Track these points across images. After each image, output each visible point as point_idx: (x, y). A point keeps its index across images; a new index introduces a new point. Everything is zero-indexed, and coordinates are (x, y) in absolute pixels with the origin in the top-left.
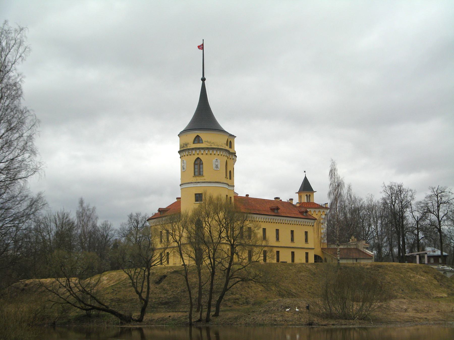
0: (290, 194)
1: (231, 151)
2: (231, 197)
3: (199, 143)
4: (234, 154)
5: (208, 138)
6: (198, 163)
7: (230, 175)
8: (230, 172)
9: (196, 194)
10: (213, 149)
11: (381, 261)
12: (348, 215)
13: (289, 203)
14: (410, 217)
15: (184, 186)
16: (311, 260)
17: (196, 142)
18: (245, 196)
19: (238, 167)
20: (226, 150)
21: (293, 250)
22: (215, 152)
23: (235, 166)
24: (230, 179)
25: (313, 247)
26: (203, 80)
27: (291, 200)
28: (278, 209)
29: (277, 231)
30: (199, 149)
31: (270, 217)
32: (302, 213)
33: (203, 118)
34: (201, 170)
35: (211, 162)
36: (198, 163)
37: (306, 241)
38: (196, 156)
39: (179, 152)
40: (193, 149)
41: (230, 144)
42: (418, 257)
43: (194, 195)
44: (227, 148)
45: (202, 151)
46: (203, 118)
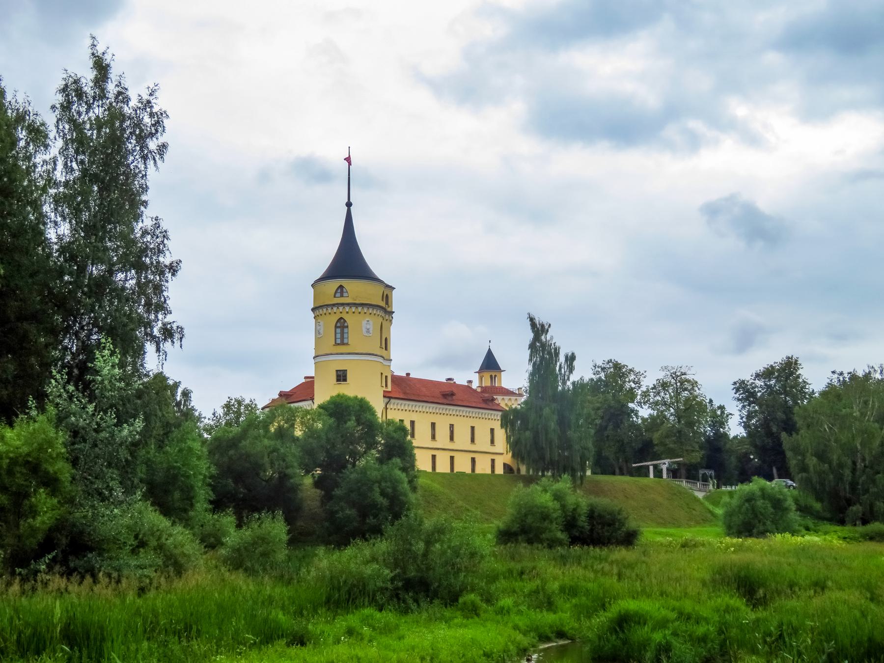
1: (389, 309)
2: (386, 377)
3: (342, 296)
5: (355, 288)
6: (341, 325)
7: (386, 344)
8: (386, 339)
9: (337, 371)
10: (362, 305)
13: (468, 388)
15: (318, 359)
16: (500, 470)
17: (338, 295)
18: (404, 375)
19: (397, 332)
21: (473, 455)
22: (371, 311)
23: (392, 328)
24: (386, 349)
25: (501, 452)
26: (349, 204)
28: (453, 394)
29: (452, 426)
30: (342, 304)
31: (442, 406)
32: (486, 401)
33: (348, 262)
34: (345, 335)
36: (341, 325)
37: (492, 442)
38: (335, 318)
39: (313, 310)
40: (334, 305)
41: (387, 299)
42: (651, 468)
43: (335, 373)
44: (383, 304)
45: (347, 309)
46: (348, 262)
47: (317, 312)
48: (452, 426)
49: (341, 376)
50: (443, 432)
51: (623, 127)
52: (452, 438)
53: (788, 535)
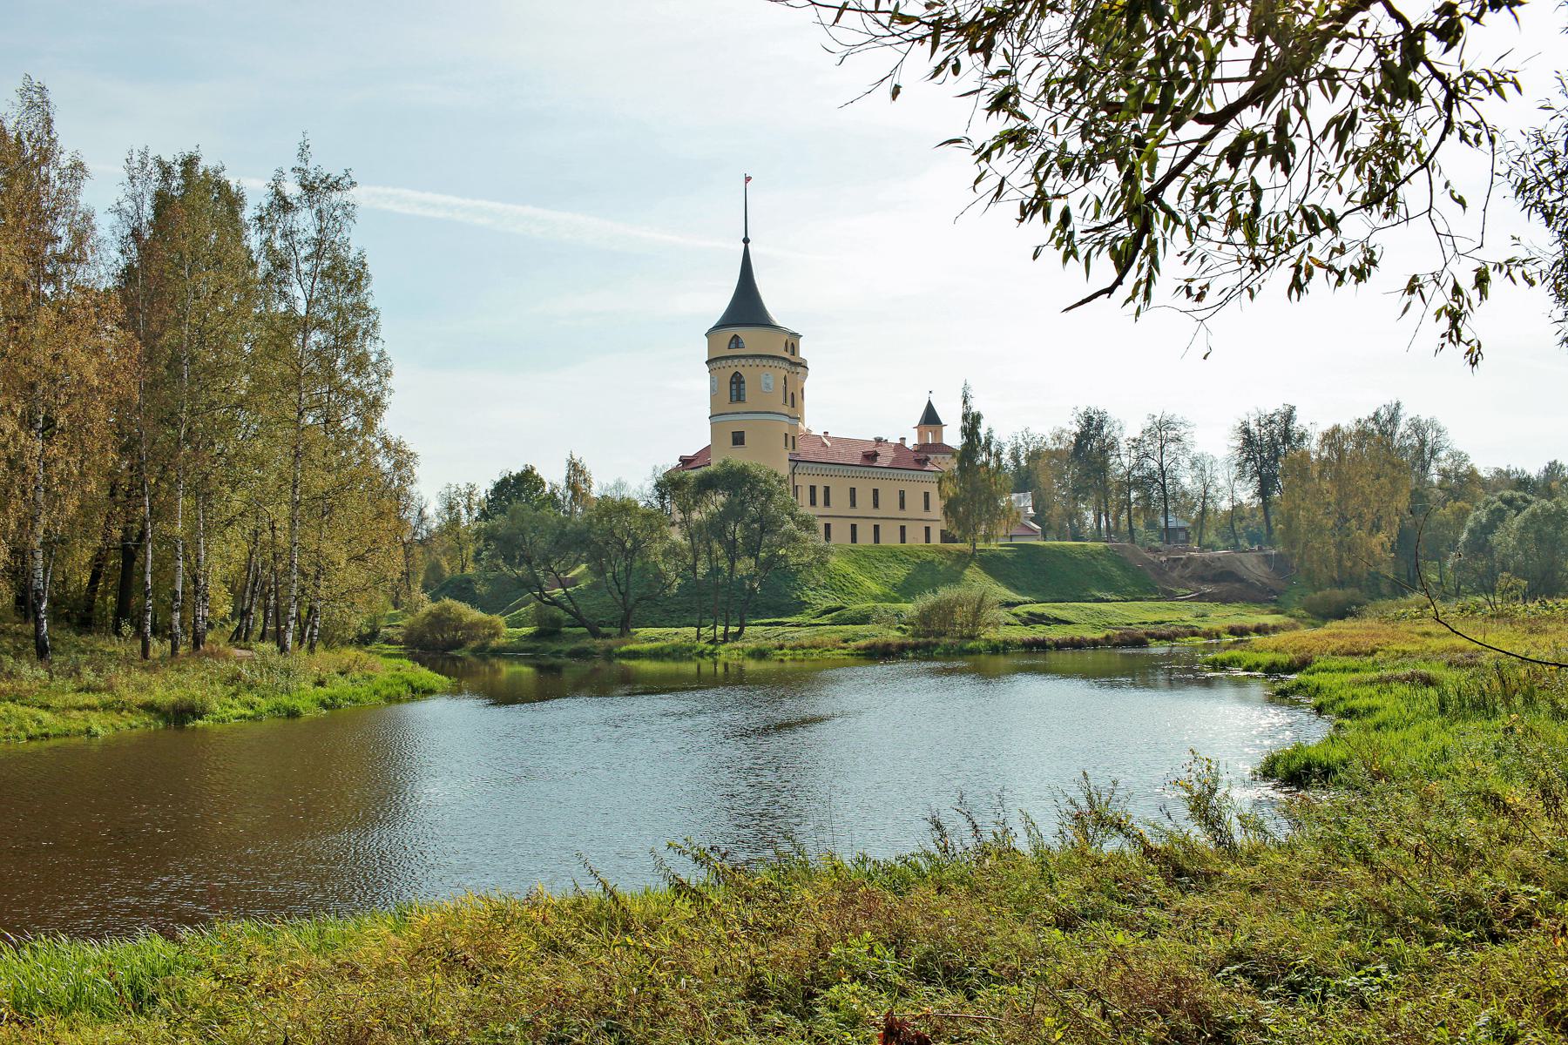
0: (904, 429)
1: (793, 359)
4: (802, 365)
5: (752, 338)
6: (737, 380)
11: (1526, 520)
12: (1023, 463)
14: (1123, 462)
20: (784, 359)
21: (854, 521)
23: (808, 385)
26: (746, 241)
27: (903, 439)
29: (876, 492)
32: (918, 461)
33: (746, 306)
35: (764, 381)
36: (737, 380)
37: (927, 507)
41: (793, 349)
44: (787, 355)
46: (746, 306)
47: (714, 365)
48: (876, 492)
49: (738, 439)
50: (864, 498)
51: (1333, 636)
52: (876, 505)
53: (244, 931)
